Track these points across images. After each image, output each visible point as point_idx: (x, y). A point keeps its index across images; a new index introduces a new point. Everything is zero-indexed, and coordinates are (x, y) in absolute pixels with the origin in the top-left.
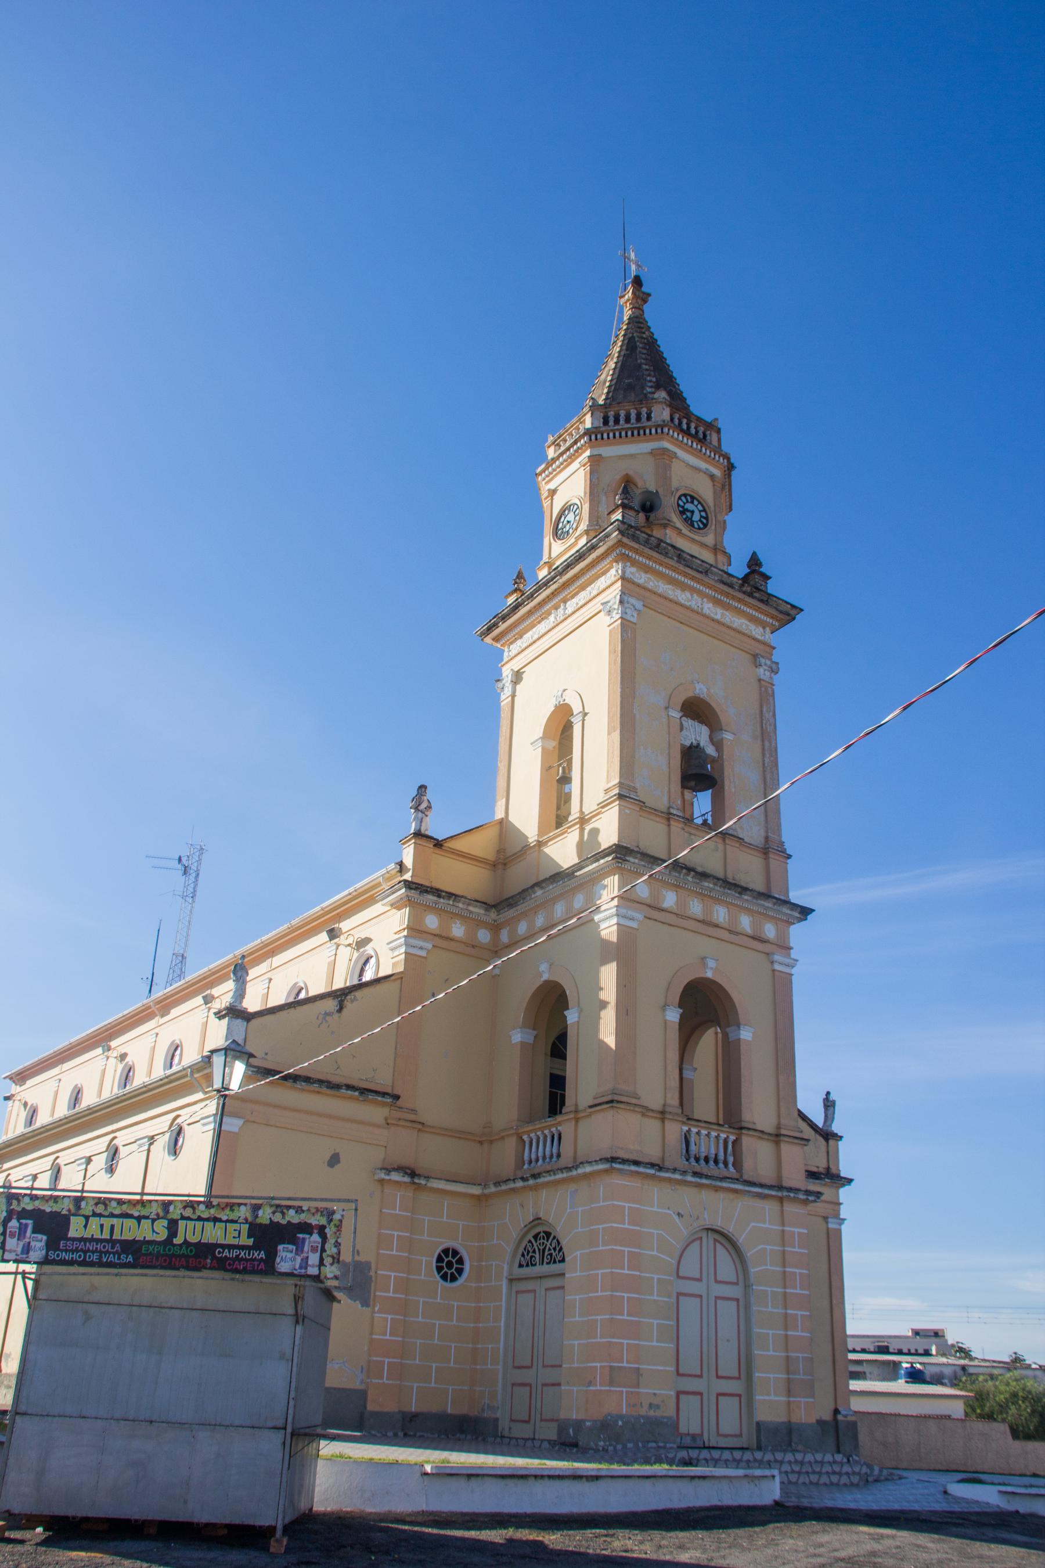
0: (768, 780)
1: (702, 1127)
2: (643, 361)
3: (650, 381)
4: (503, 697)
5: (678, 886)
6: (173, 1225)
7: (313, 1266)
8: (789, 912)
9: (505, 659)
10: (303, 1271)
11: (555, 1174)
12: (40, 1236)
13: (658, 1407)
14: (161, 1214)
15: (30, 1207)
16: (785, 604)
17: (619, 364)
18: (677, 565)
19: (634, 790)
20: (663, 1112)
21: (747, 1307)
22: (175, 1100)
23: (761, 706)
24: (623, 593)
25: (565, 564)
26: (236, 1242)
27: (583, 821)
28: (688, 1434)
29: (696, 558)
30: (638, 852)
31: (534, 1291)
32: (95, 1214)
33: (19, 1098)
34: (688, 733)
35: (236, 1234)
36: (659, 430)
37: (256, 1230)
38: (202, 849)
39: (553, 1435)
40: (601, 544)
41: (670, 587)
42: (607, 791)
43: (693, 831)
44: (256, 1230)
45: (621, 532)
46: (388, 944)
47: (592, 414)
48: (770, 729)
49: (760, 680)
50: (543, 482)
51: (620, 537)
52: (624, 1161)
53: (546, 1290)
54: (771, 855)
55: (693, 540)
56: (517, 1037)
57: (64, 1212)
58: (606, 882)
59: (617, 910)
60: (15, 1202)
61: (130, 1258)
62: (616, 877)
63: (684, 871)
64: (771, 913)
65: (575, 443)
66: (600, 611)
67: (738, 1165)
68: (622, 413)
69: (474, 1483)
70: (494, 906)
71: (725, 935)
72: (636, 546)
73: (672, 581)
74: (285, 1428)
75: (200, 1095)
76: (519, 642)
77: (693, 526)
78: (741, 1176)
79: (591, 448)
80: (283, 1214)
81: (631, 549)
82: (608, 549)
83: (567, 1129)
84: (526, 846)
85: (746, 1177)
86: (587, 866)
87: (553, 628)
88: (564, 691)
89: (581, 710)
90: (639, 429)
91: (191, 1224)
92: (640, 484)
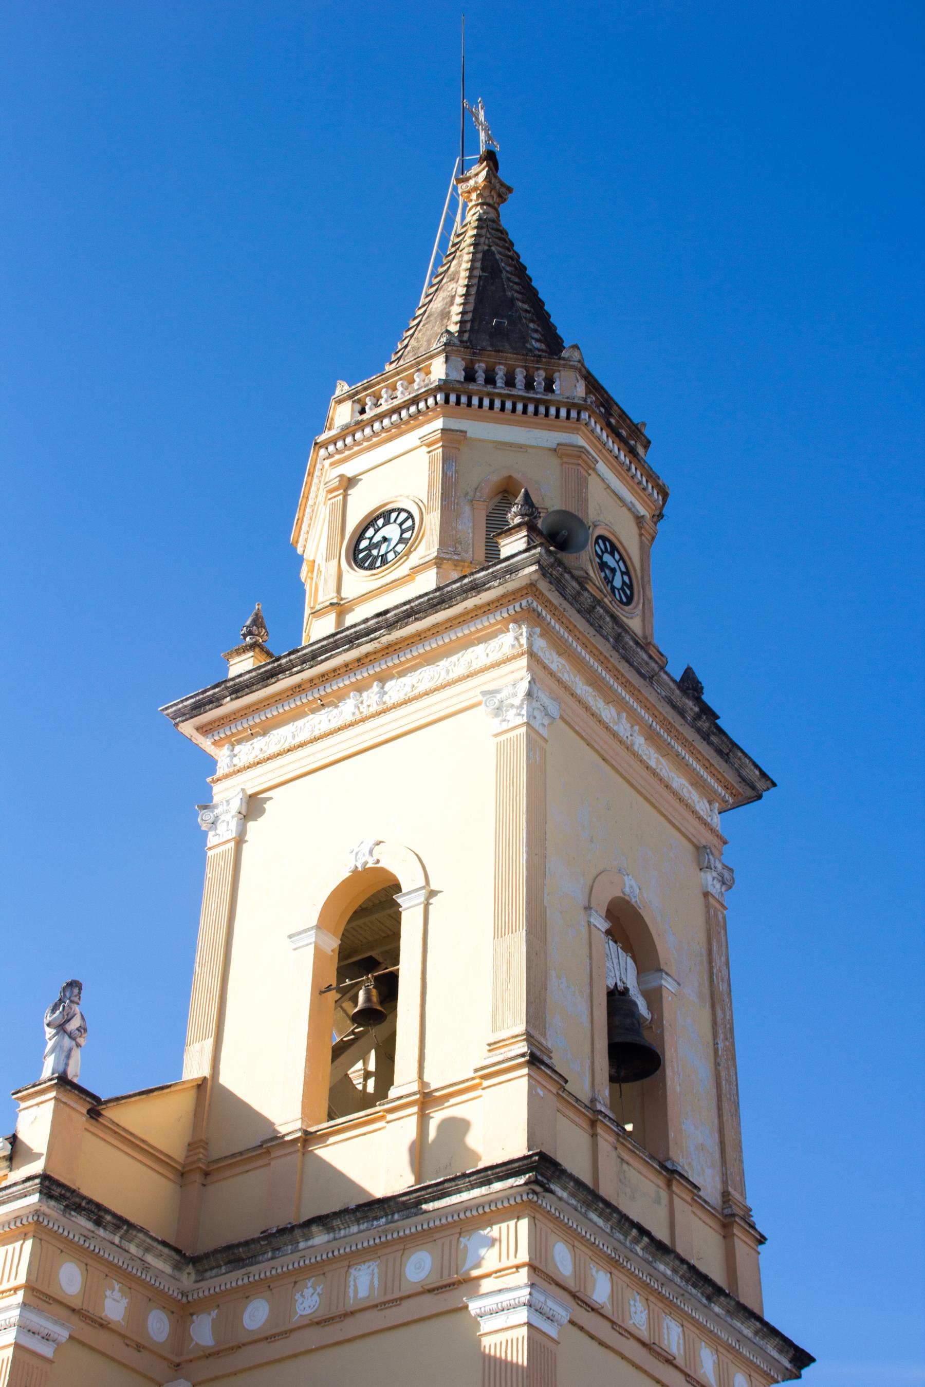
2: (516, 295)
4: (212, 840)
16: (752, 767)
25: (405, 608)
36: (574, 414)
40: (496, 583)
42: (493, 1046)
45: (543, 571)
49: (706, 894)
58: (494, 1231)
59: (530, 1294)
62: (524, 1224)
66: (478, 704)
70: (195, 1260)
72: (555, 598)
73: (595, 682)
76: (259, 742)
81: (547, 604)
84: (276, 1138)
86: (459, 1191)
88: (378, 843)
89: (423, 883)
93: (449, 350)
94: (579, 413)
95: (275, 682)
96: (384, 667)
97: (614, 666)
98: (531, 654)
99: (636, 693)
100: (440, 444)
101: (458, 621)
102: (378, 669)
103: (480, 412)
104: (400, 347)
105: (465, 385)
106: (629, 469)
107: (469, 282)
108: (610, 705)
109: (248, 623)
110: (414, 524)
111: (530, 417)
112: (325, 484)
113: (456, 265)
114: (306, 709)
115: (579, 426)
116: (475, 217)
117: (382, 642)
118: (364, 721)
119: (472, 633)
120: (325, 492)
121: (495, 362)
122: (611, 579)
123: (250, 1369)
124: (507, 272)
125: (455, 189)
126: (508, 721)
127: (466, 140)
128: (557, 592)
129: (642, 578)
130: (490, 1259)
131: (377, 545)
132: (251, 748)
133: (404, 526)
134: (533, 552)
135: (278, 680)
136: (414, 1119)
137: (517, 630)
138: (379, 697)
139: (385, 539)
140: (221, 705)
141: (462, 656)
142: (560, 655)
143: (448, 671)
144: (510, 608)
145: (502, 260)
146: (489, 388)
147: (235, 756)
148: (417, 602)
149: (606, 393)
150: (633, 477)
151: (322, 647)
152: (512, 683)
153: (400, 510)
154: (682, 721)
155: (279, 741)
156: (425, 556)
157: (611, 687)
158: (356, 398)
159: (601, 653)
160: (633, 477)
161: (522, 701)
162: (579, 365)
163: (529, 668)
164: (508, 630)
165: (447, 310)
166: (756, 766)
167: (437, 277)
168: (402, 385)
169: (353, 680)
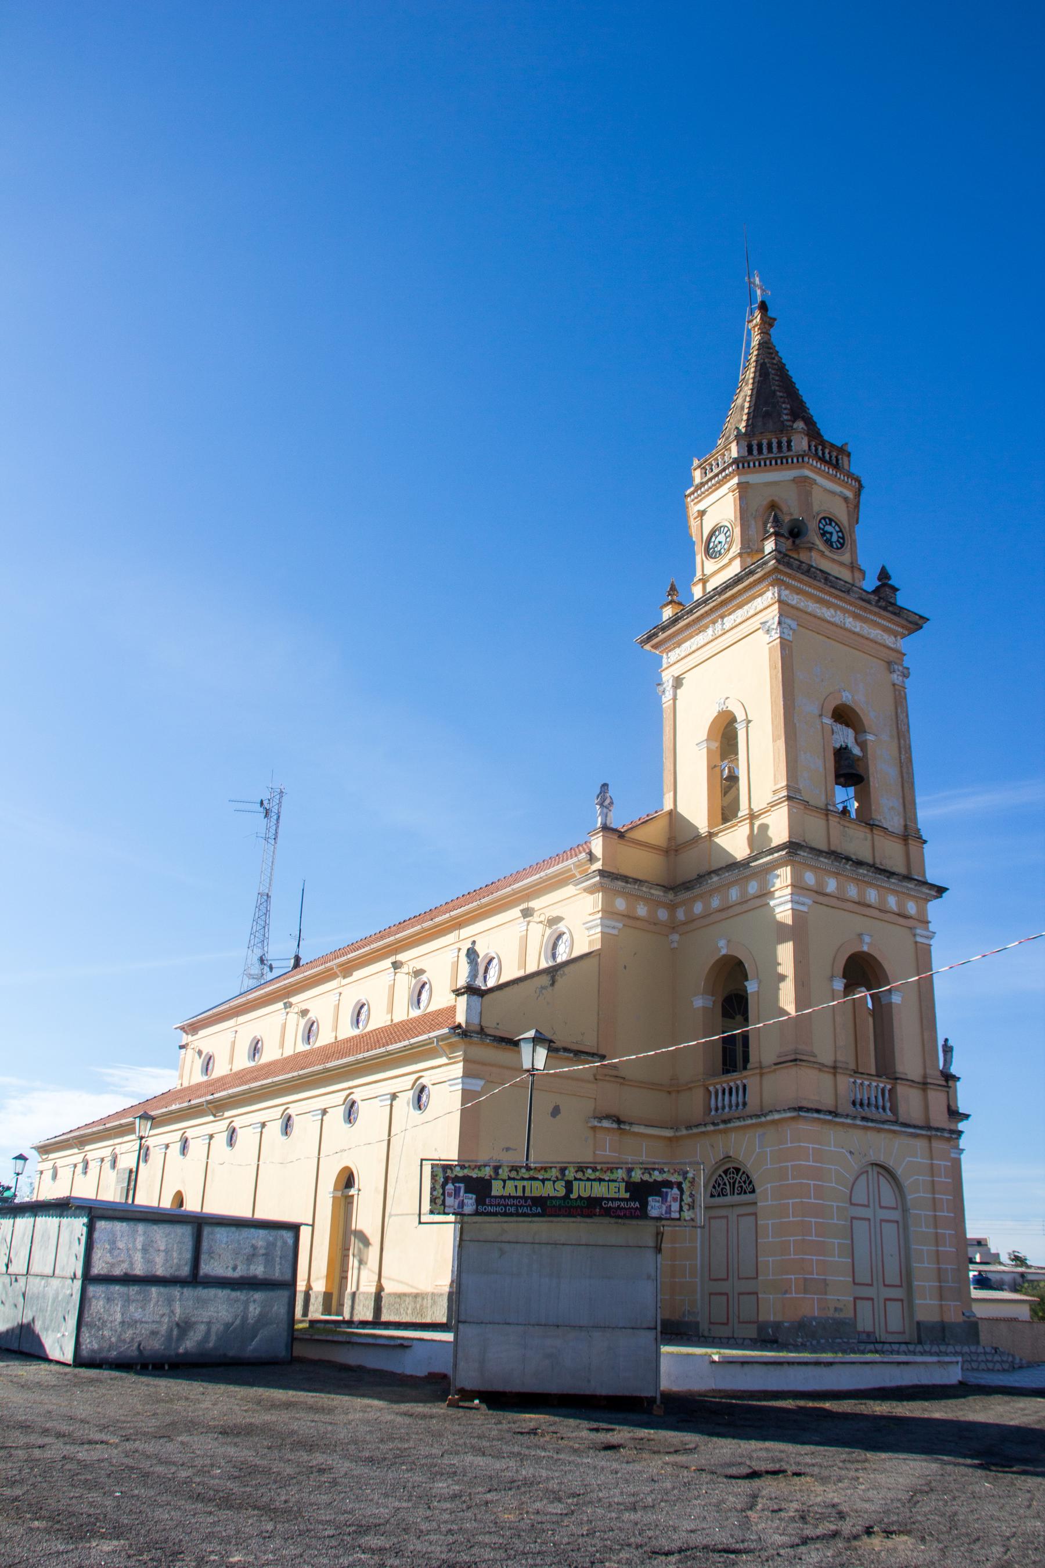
0: (905, 775)
1: (865, 1079)
2: (777, 388)
3: (785, 409)
4: (664, 700)
5: (838, 874)
6: (569, 1186)
7: (675, 1212)
8: (927, 891)
9: (665, 666)
10: (668, 1215)
11: (744, 1120)
12: (470, 1195)
13: (841, 1310)
14: (560, 1177)
15: (460, 1174)
17: (755, 390)
18: (823, 586)
19: (799, 791)
20: (835, 1068)
21: (906, 1227)
22: (416, 1063)
23: (896, 708)
24: (781, 615)
26: (616, 1196)
27: (752, 817)
28: (864, 1332)
29: (840, 579)
30: (807, 847)
31: (727, 1217)
32: (510, 1178)
33: (192, 1046)
34: (838, 737)
35: (617, 1190)
36: (800, 460)
37: (630, 1186)
38: (281, 792)
39: (754, 1335)
41: (818, 605)
42: (775, 792)
43: (847, 824)
44: (630, 1186)
45: (778, 561)
46: (584, 924)
47: (737, 443)
48: (904, 728)
49: (894, 685)
50: (692, 503)
51: (776, 564)
52: (808, 1110)
53: (738, 1216)
54: (910, 842)
55: (833, 560)
56: (699, 1002)
57: (487, 1177)
58: (778, 872)
60: (449, 1171)
61: (539, 1210)
62: (789, 868)
63: (844, 861)
64: (912, 893)
65: (724, 470)
66: (759, 629)
67: (894, 1109)
68: (765, 442)
69: (747, 1368)
71: (875, 913)
72: (789, 571)
74: (656, 1328)
75: (444, 1060)
76: (677, 650)
77: (831, 546)
78: (898, 1119)
79: (738, 475)
80: (650, 1174)
82: (765, 574)
83: (752, 1081)
85: (901, 1120)
86: (762, 858)
87: (712, 641)
88: (727, 698)
90: (782, 458)
91: (582, 1183)
92: (785, 509)
93: (739, 437)
123: (713, 923)
127: (751, 294)
130: (778, 883)
136: (748, 825)
150: (839, 479)
166: (916, 614)
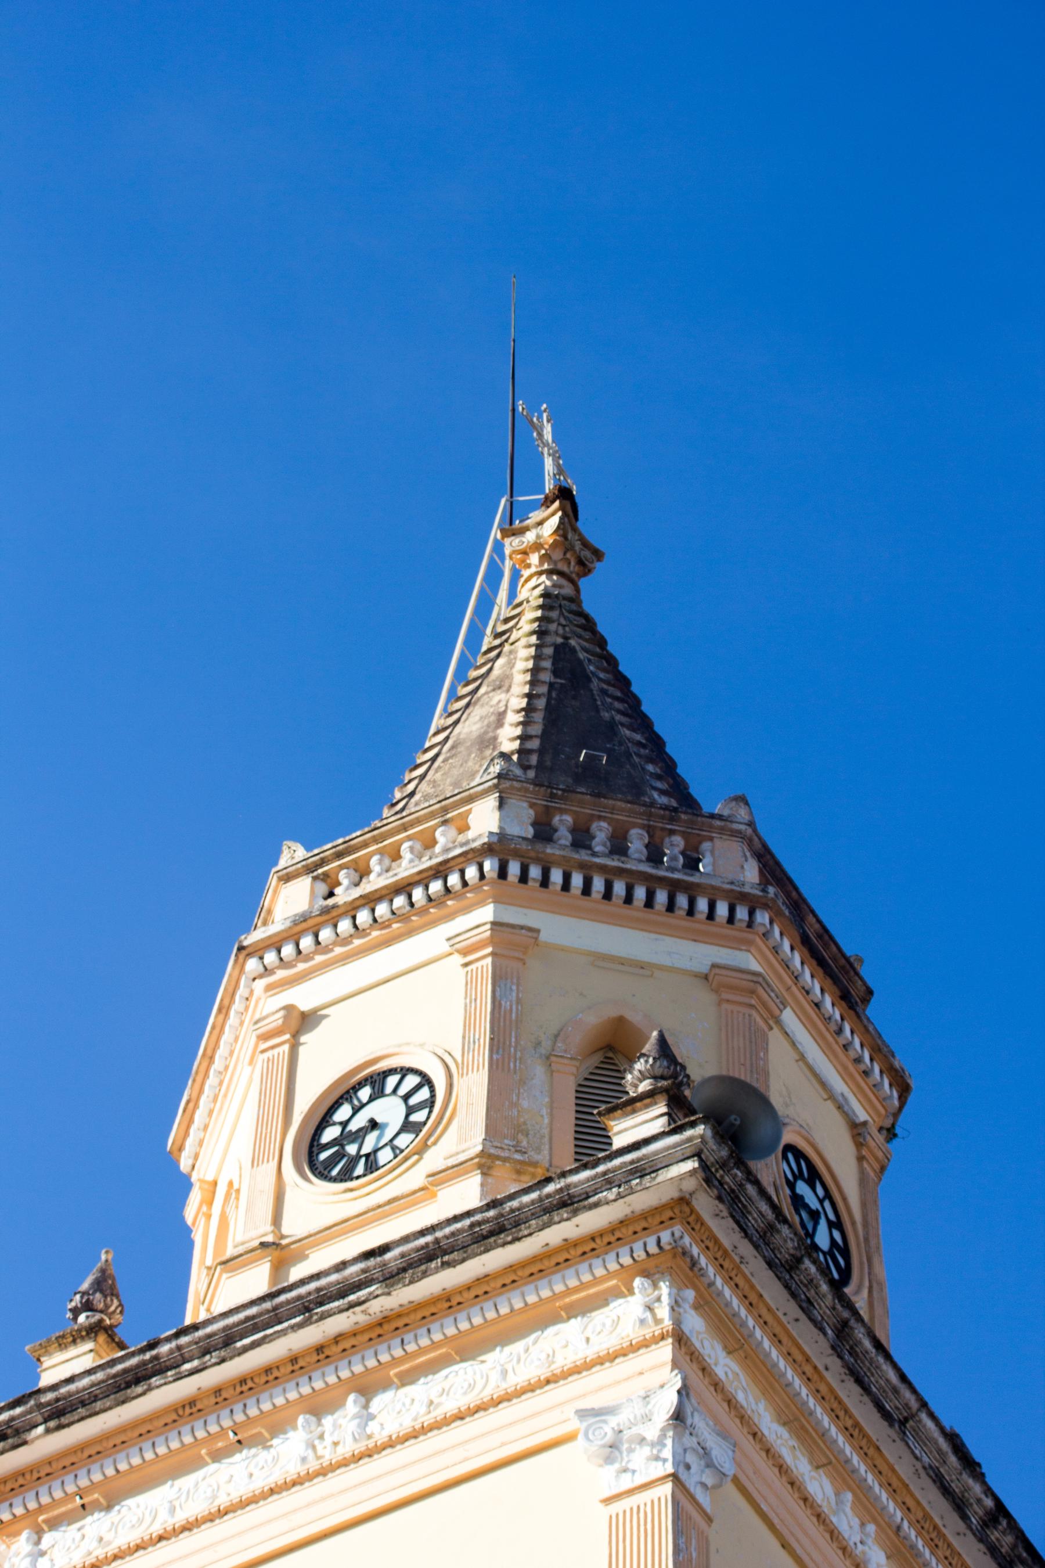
2: (618, 718)
25: (422, 1241)
29: (888, 1357)
36: (742, 913)
40: (612, 1194)
45: (707, 1173)
66: (569, 1438)
76: (96, 1524)
81: (710, 1243)
94: (751, 913)
95: (144, 1393)
96: (371, 1363)
97: (832, 1390)
98: (680, 1339)
99: (871, 1452)
100: (489, 950)
101: (528, 1271)
102: (358, 1368)
103: (564, 898)
104: (398, 795)
105: (539, 846)
106: (840, 1031)
107: (531, 690)
108: (821, 1471)
109: (85, 1286)
110: (433, 1095)
111: (659, 913)
112: (256, 1023)
113: (503, 666)
114: (203, 1452)
115: (750, 936)
116: (538, 591)
117: (371, 1311)
118: (325, 1475)
119: (555, 1297)
120: (254, 1039)
121: (593, 815)
122: (810, 1230)
124: (600, 679)
125: (499, 547)
126: (634, 1472)
128: (730, 1220)
129: (867, 1240)
131: (359, 1136)
132: (78, 1536)
133: (413, 1101)
134: (689, 1133)
135: (150, 1389)
137: (650, 1290)
138: (359, 1426)
139: (373, 1125)
140: (25, 1443)
141: (535, 1342)
142: (730, 1352)
143: (504, 1373)
144: (638, 1247)
145: (589, 660)
146: (583, 856)
147: (42, 1554)
148: (447, 1230)
149: (796, 889)
151: (248, 1319)
152: (642, 1393)
153: (405, 1072)
154: (961, 1526)
155: (141, 1521)
156: (457, 1153)
157: (823, 1434)
158: (320, 871)
159: (808, 1360)
160: (846, 1047)
161: (664, 1430)
162: (749, 831)
163: (675, 1364)
164: (631, 1292)
165: (491, 734)
167: (467, 684)
168: (412, 849)
169: (306, 1390)
